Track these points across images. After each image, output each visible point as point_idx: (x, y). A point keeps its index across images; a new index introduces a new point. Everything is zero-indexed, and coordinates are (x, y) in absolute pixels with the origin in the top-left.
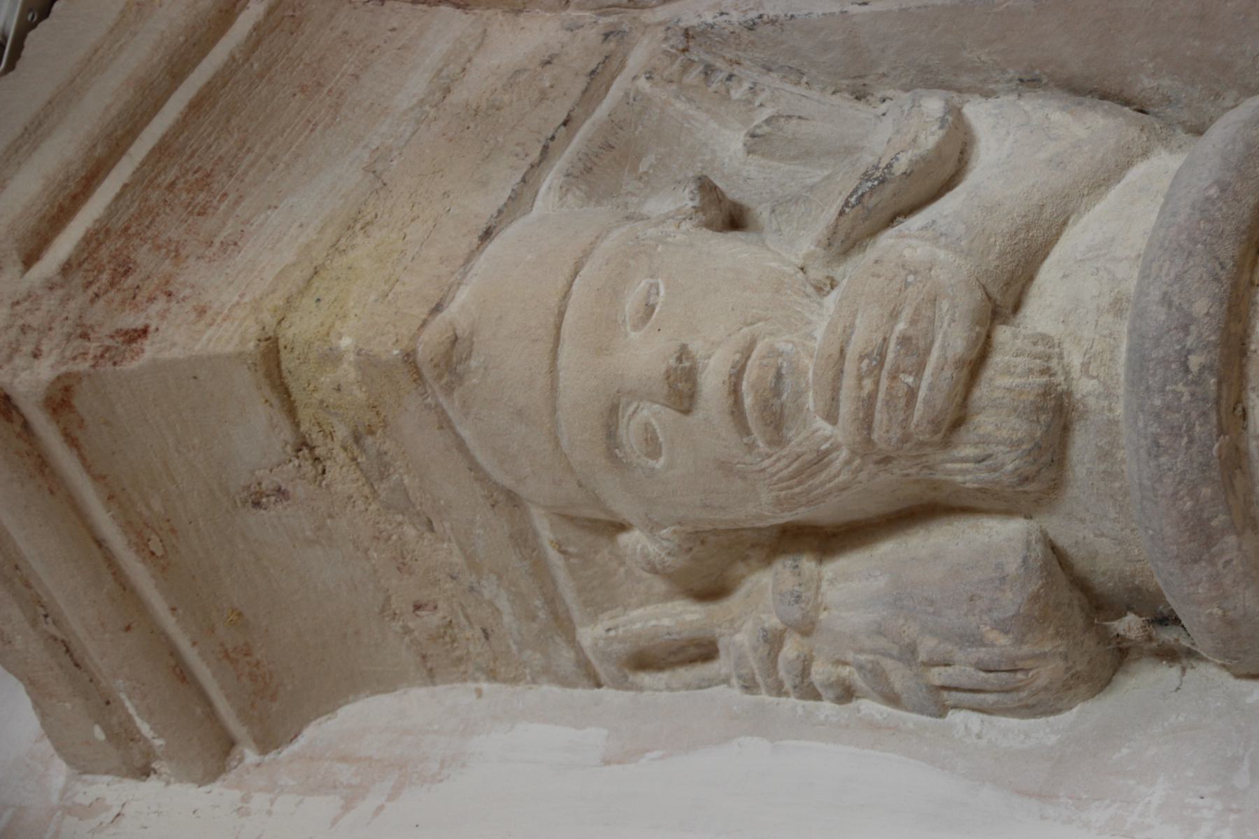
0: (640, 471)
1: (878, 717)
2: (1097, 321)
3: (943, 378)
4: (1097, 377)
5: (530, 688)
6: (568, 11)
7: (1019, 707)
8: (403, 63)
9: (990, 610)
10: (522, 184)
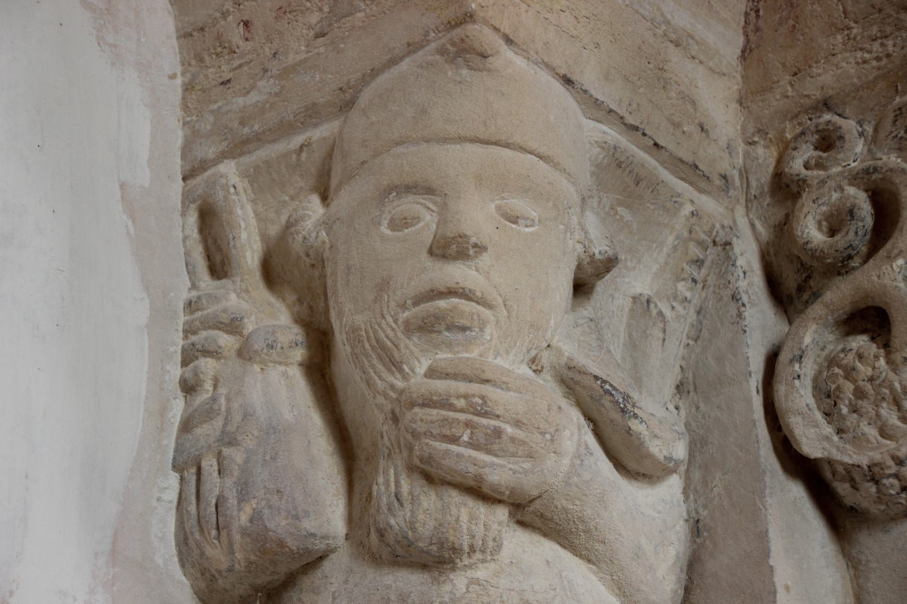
0: (378, 214)
1: (171, 415)
2: (513, 590)
3: (467, 465)
4: (468, 592)
5: (179, 120)
6: (742, 145)
7: (186, 532)
8: (698, 6)
9: (270, 507)
10: (608, 110)
